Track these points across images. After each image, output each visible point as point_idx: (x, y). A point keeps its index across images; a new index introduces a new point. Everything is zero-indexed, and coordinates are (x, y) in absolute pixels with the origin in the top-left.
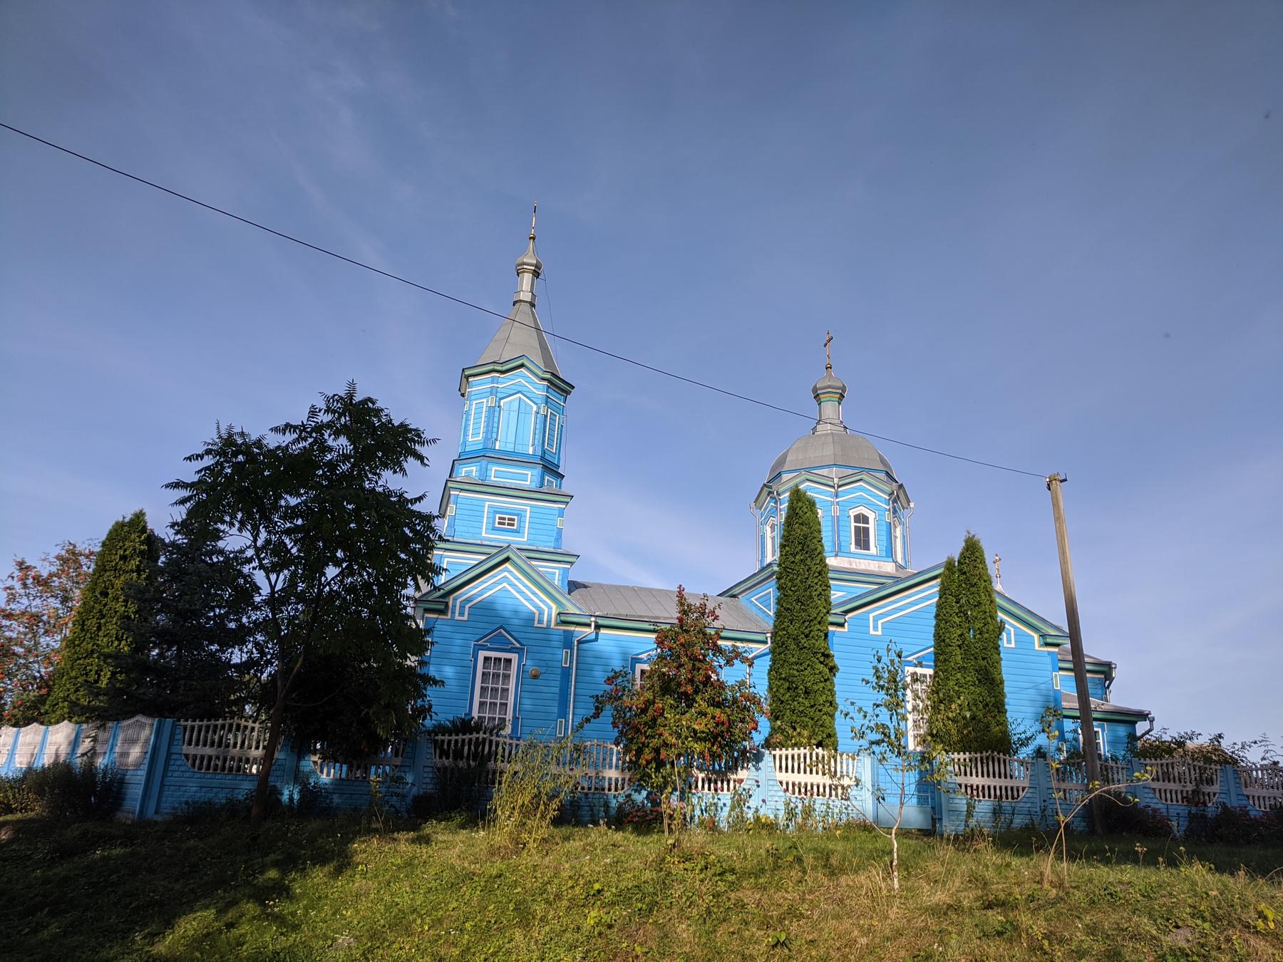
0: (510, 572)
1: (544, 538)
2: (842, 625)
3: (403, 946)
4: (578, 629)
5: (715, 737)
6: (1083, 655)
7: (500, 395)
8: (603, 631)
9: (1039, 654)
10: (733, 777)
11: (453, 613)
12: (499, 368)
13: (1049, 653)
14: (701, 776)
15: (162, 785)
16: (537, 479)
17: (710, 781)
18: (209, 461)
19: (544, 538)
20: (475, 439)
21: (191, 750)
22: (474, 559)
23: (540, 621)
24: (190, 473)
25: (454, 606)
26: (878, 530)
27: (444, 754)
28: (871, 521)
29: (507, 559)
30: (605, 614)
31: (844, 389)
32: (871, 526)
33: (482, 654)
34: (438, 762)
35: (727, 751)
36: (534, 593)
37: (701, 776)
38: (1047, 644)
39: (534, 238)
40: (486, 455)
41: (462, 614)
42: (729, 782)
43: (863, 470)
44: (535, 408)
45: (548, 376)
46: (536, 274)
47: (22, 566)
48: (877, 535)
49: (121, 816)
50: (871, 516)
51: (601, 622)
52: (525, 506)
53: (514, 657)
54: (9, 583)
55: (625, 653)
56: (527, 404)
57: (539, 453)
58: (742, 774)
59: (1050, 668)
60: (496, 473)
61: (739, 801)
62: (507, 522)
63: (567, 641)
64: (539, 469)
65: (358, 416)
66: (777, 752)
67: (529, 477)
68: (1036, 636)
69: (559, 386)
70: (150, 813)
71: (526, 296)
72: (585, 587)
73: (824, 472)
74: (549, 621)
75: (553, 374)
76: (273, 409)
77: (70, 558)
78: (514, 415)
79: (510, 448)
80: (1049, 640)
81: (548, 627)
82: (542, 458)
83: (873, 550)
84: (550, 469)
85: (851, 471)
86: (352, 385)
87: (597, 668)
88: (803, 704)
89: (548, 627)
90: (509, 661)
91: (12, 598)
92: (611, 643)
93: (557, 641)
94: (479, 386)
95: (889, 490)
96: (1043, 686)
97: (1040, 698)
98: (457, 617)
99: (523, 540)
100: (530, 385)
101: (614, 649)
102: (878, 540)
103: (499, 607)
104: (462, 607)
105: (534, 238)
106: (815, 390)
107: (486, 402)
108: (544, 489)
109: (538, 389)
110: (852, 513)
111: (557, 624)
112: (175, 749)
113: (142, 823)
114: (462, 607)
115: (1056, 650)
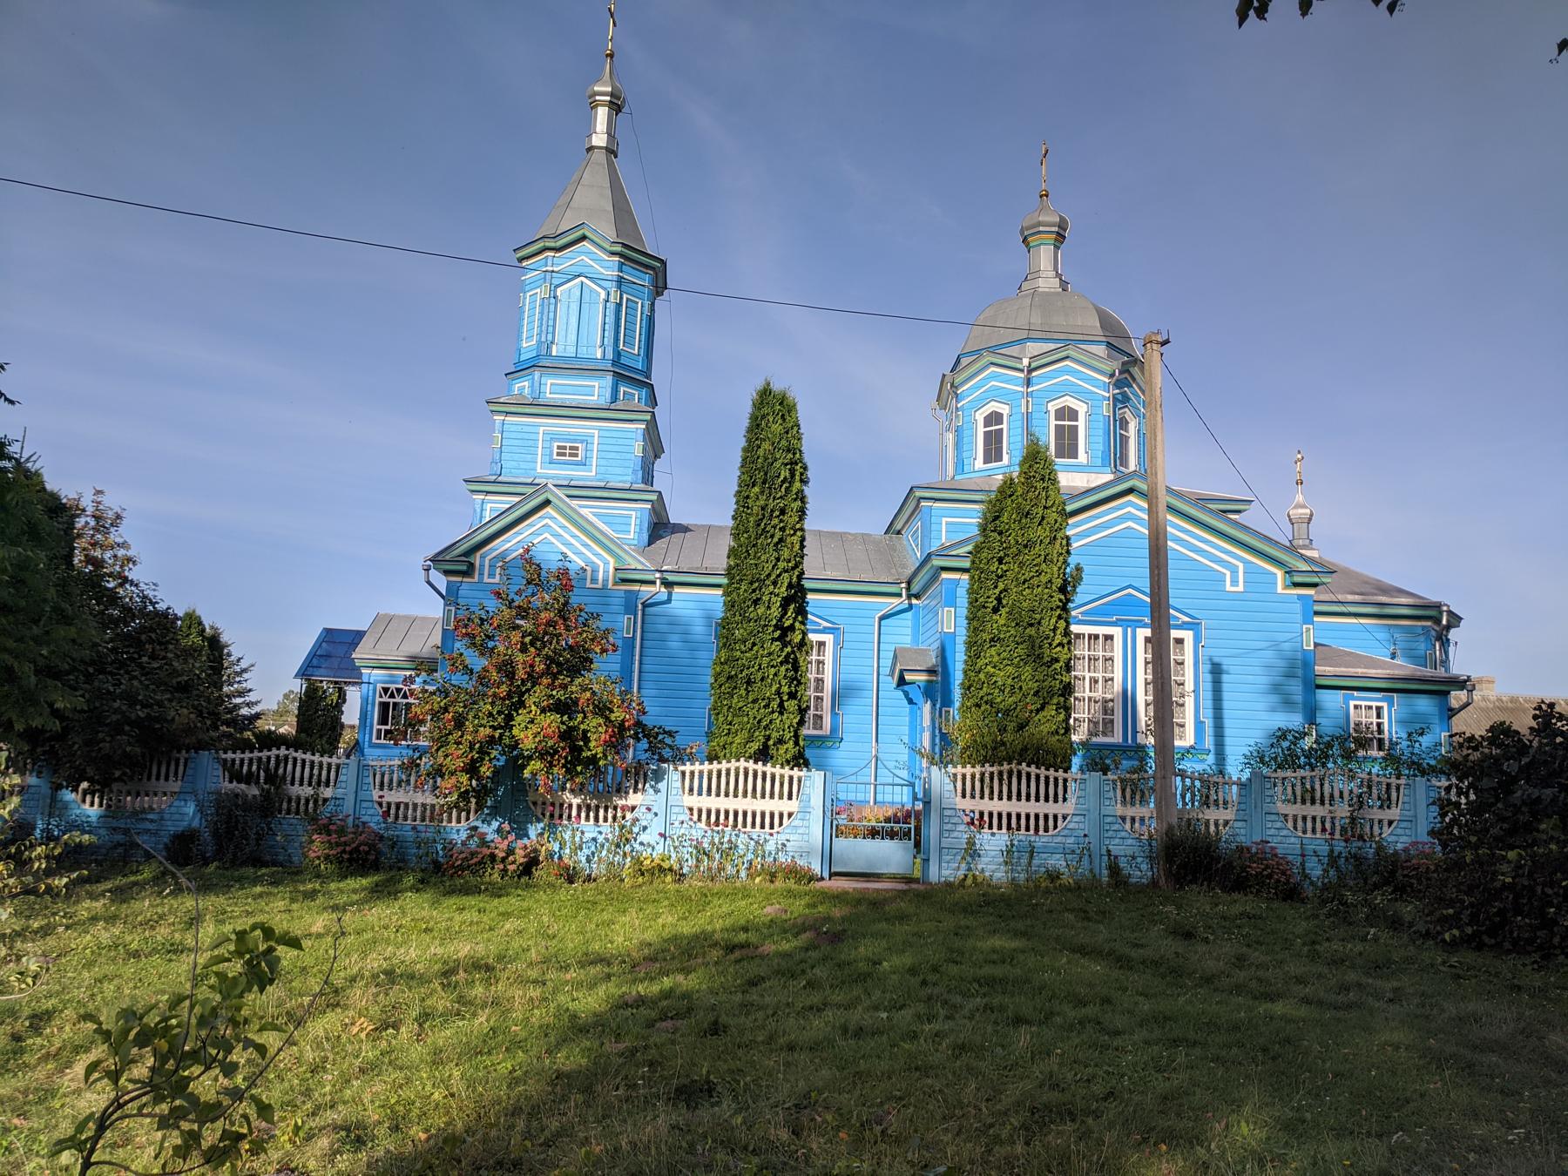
0: (552, 518)
1: (618, 470)
4: (644, 588)
6: (1168, 606)
7: (556, 282)
8: (677, 590)
9: (1284, 600)
10: (621, 803)
11: (481, 574)
12: (552, 244)
14: (576, 801)
16: (608, 394)
17: (588, 808)
19: (618, 470)
20: (528, 345)
22: (503, 503)
23: (594, 580)
25: (482, 566)
26: (1088, 428)
27: (236, 776)
28: (1081, 417)
29: (547, 503)
30: (675, 568)
31: (1062, 225)
32: (1081, 424)
34: (228, 786)
36: (586, 545)
37: (576, 801)
38: (1296, 585)
39: (611, 56)
41: (491, 575)
42: (615, 808)
43: (1068, 342)
44: (603, 295)
45: (618, 248)
46: (616, 107)
50: (1082, 409)
51: (671, 578)
52: (592, 429)
55: (709, 617)
56: (592, 290)
57: (610, 355)
58: (633, 799)
59: (1299, 617)
60: (553, 388)
62: (568, 452)
63: (630, 604)
64: (609, 378)
66: (688, 768)
67: (597, 390)
68: (1279, 574)
69: (645, 268)
71: (599, 140)
72: (685, 529)
74: (605, 580)
75: (624, 245)
78: (575, 307)
79: (571, 352)
80: (1298, 579)
81: (605, 587)
83: (1082, 457)
85: (1052, 346)
87: (675, 637)
88: (766, 701)
89: (605, 587)
92: (691, 605)
93: (617, 603)
95: (1108, 369)
96: (1286, 646)
97: (1282, 663)
98: (486, 580)
101: (697, 613)
102: (1088, 443)
105: (611, 56)
107: (541, 292)
108: (620, 405)
109: (607, 267)
110: (1053, 407)
111: (615, 584)
115: (1311, 592)
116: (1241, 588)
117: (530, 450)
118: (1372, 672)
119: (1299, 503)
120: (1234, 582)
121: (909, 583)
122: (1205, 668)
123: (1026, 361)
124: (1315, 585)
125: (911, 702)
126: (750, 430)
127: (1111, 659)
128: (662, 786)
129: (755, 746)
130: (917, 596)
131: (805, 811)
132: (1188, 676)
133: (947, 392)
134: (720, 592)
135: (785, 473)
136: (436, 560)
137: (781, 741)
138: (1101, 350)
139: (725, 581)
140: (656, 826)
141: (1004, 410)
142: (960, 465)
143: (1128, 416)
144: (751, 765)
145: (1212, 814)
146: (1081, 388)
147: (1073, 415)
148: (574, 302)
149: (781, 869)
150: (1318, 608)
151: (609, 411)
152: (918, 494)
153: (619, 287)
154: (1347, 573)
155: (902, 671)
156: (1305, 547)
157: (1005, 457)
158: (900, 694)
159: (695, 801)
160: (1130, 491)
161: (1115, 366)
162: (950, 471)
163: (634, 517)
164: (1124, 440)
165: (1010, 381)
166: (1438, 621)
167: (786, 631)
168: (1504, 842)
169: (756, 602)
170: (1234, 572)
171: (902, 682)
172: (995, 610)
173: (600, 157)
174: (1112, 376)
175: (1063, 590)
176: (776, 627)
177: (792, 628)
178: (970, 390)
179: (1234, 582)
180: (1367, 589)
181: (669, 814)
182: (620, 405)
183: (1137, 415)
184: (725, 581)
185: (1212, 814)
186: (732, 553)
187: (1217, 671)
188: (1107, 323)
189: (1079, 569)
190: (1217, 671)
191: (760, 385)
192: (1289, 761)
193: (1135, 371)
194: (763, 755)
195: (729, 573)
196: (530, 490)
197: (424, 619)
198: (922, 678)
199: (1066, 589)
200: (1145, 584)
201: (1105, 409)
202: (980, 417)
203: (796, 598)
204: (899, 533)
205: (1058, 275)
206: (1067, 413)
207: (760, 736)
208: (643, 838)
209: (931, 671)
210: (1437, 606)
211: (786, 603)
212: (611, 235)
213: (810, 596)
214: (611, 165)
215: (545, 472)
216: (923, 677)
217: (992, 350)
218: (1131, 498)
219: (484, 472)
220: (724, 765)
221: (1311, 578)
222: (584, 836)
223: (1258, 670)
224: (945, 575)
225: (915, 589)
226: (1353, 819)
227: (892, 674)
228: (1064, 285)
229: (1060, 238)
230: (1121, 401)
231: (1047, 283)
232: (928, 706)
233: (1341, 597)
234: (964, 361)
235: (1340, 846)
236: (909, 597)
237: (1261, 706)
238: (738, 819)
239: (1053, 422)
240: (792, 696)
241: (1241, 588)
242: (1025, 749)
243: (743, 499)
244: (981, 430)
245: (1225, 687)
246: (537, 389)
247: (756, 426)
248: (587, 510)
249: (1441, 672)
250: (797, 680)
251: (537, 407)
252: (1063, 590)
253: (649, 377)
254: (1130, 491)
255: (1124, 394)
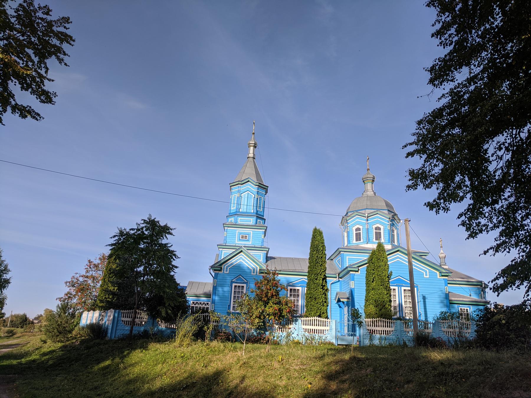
1: (258, 242)
2: (358, 271)
3: (255, 397)
5: (276, 314)
9: (440, 280)
13: (444, 279)
15: (116, 329)
16: (255, 221)
18: (117, 238)
19: (258, 242)
20: (233, 208)
21: (124, 319)
24: (113, 241)
26: (384, 233)
29: (242, 251)
31: (374, 178)
32: (382, 231)
33: (234, 285)
35: (287, 317)
38: (443, 276)
40: (237, 214)
41: (227, 271)
43: (378, 210)
44: (253, 196)
45: (258, 184)
46: (255, 147)
47: (90, 262)
48: (384, 234)
49: (106, 338)
50: (382, 227)
53: (245, 285)
54: (87, 267)
57: (255, 212)
59: (444, 285)
60: (241, 220)
61: (289, 335)
62: (244, 237)
64: (255, 218)
65: (152, 224)
66: (303, 319)
67: (252, 221)
68: (438, 273)
69: (263, 187)
70: (113, 337)
71: (251, 155)
72: (274, 258)
73: (363, 212)
76: (132, 222)
77: (102, 259)
78: (246, 199)
79: (245, 211)
80: (443, 274)
82: (257, 213)
84: (260, 217)
85: (373, 211)
86: (150, 215)
90: (243, 287)
91: (87, 272)
94: (235, 189)
95: (389, 217)
99: (249, 243)
100: (252, 187)
102: (384, 237)
103: (241, 266)
104: (227, 269)
106: (363, 179)
107: (237, 195)
108: (258, 225)
109: (254, 189)
110: (374, 227)
112: (119, 319)
113: (111, 340)
114: (227, 269)
115: (446, 278)
116: (428, 277)
117: (234, 237)
118: (464, 299)
119: (442, 253)
120: (426, 275)
121: (339, 274)
122: (421, 298)
123: (366, 215)
124: (447, 276)
125: (340, 307)
126: (312, 238)
127: (395, 295)
128: (297, 323)
129: (318, 314)
130: (341, 278)
131: (331, 329)
132: (418, 298)
133: (344, 220)
134: (306, 277)
135: (322, 249)
136: (212, 267)
137: (323, 313)
138: (386, 212)
139: (307, 274)
140: (296, 333)
141: (361, 227)
142: (349, 241)
143: (394, 229)
144: (318, 318)
145: (427, 331)
146: (382, 222)
147: (380, 229)
148: (246, 197)
149: (327, 343)
150: (449, 282)
151: (255, 226)
152: (340, 250)
153: (258, 194)
154: (456, 273)
155: (339, 298)
156: (444, 265)
157: (362, 240)
158: (337, 305)
159: (305, 327)
160: (398, 251)
161: (390, 216)
162: (346, 244)
163: (261, 256)
164: (393, 235)
165: (363, 220)
166: (482, 286)
167: (324, 286)
168: (488, 330)
169: (316, 279)
170: (426, 272)
171: (339, 301)
172: (373, 282)
173: (251, 159)
174: (390, 219)
175: (388, 277)
176: (322, 285)
177: (325, 286)
178: (351, 222)
179: (426, 275)
180: (463, 276)
181: (298, 330)
182: (258, 225)
183: (396, 229)
184: (307, 274)
185: (427, 331)
186: (309, 267)
187: (424, 298)
188: (388, 205)
189: (391, 272)
190: (424, 298)
191: (314, 227)
192: (444, 319)
193: (396, 217)
194: (320, 316)
195: (308, 272)
196: (238, 248)
197: (202, 283)
198: (345, 300)
199: (389, 277)
200: (408, 278)
201: (388, 228)
202: (354, 229)
203: (325, 278)
204: (332, 260)
205: (373, 191)
206: (378, 228)
207: (319, 311)
208: (293, 335)
209: (348, 298)
210: (481, 282)
211: (323, 279)
212: (256, 181)
213: (327, 278)
214: (254, 161)
215: (238, 243)
216: (346, 300)
217: (357, 211)
218: (398, 252)
219: (222, 242)
220: (309, 318)
221: (446, 274)
222: (279, 334)
223: (437, 296)
224: (351, 272)
225: (341, 276)
226: (460, 332)
227: (335, 300)
228: (375, 193)
229: (373, 181)
230: (392, 225)
231: (370, 193)
232: (347, 308)
233: (455, 279)
234: (349, 214)
235: (457, 338)
236: (339, 278)
237: (439, 306)
238: (314, 331)
239: (374, 231)
240: (325, 302)
241: (428, 277)
242: (382, 315)
243: (311, 255)
244: (355, 232)
245: (427, 303)
246: (236, 220)
247: (314, 237)
248: (252, 253)
249: (484, 300)
250: (326, 299)
251: (236, 225)
252: (388, 277)
253: (263, 216)
254: (398, 251)
255: (393, 223)
